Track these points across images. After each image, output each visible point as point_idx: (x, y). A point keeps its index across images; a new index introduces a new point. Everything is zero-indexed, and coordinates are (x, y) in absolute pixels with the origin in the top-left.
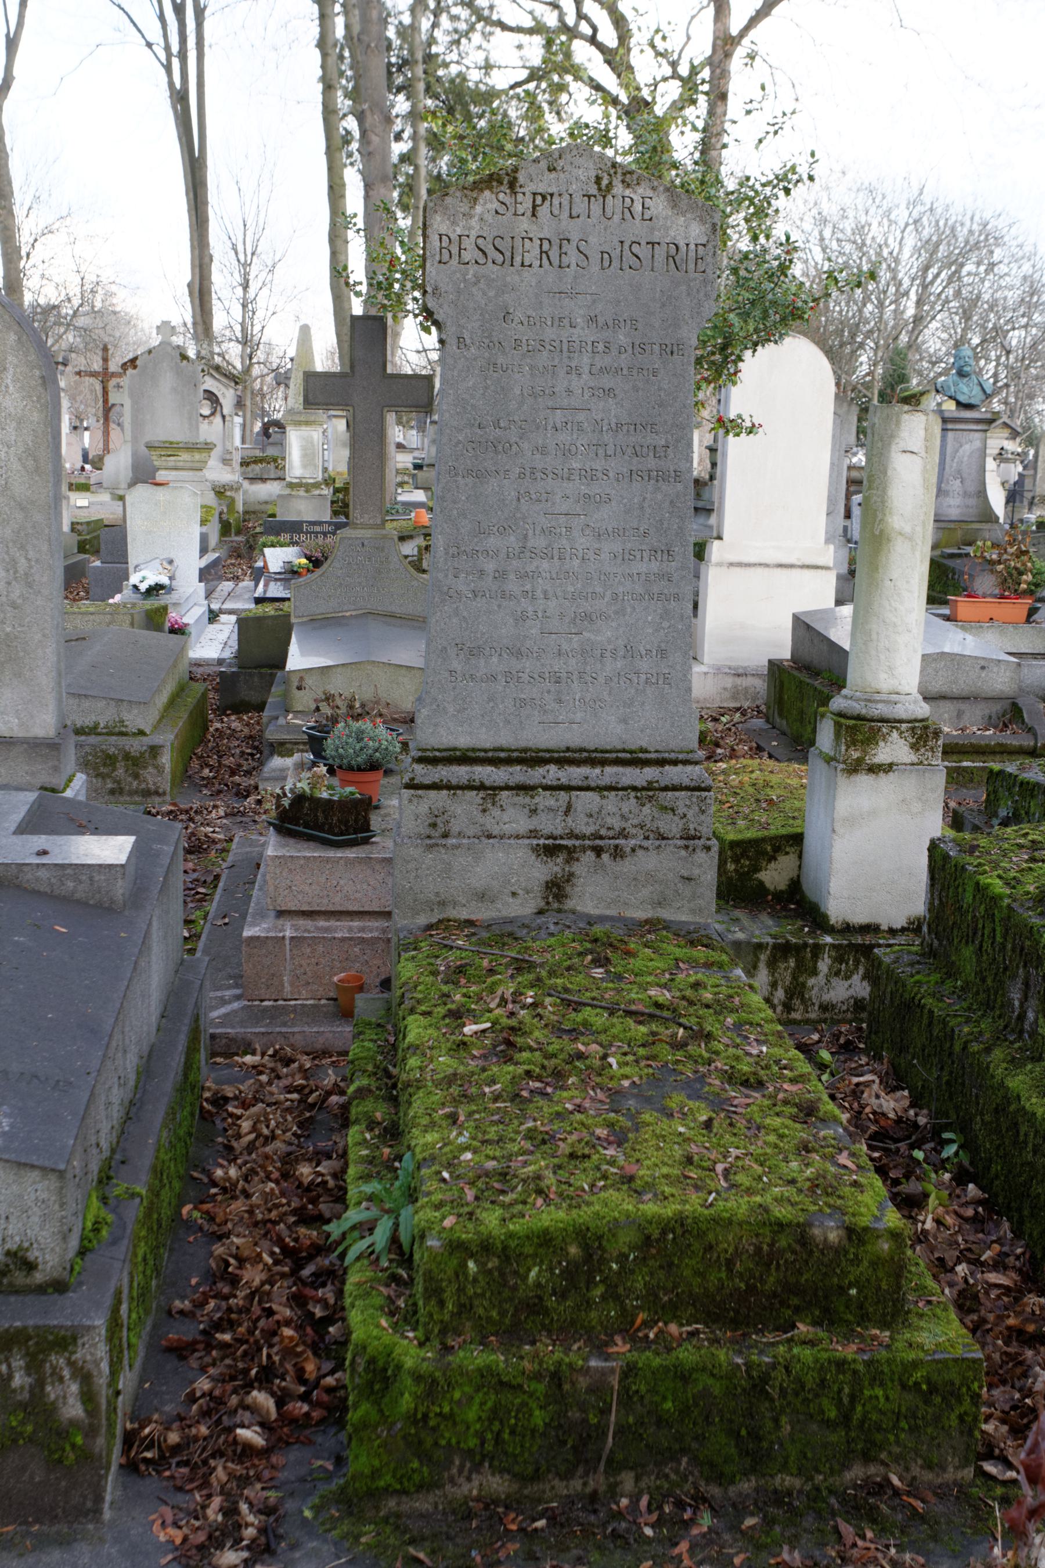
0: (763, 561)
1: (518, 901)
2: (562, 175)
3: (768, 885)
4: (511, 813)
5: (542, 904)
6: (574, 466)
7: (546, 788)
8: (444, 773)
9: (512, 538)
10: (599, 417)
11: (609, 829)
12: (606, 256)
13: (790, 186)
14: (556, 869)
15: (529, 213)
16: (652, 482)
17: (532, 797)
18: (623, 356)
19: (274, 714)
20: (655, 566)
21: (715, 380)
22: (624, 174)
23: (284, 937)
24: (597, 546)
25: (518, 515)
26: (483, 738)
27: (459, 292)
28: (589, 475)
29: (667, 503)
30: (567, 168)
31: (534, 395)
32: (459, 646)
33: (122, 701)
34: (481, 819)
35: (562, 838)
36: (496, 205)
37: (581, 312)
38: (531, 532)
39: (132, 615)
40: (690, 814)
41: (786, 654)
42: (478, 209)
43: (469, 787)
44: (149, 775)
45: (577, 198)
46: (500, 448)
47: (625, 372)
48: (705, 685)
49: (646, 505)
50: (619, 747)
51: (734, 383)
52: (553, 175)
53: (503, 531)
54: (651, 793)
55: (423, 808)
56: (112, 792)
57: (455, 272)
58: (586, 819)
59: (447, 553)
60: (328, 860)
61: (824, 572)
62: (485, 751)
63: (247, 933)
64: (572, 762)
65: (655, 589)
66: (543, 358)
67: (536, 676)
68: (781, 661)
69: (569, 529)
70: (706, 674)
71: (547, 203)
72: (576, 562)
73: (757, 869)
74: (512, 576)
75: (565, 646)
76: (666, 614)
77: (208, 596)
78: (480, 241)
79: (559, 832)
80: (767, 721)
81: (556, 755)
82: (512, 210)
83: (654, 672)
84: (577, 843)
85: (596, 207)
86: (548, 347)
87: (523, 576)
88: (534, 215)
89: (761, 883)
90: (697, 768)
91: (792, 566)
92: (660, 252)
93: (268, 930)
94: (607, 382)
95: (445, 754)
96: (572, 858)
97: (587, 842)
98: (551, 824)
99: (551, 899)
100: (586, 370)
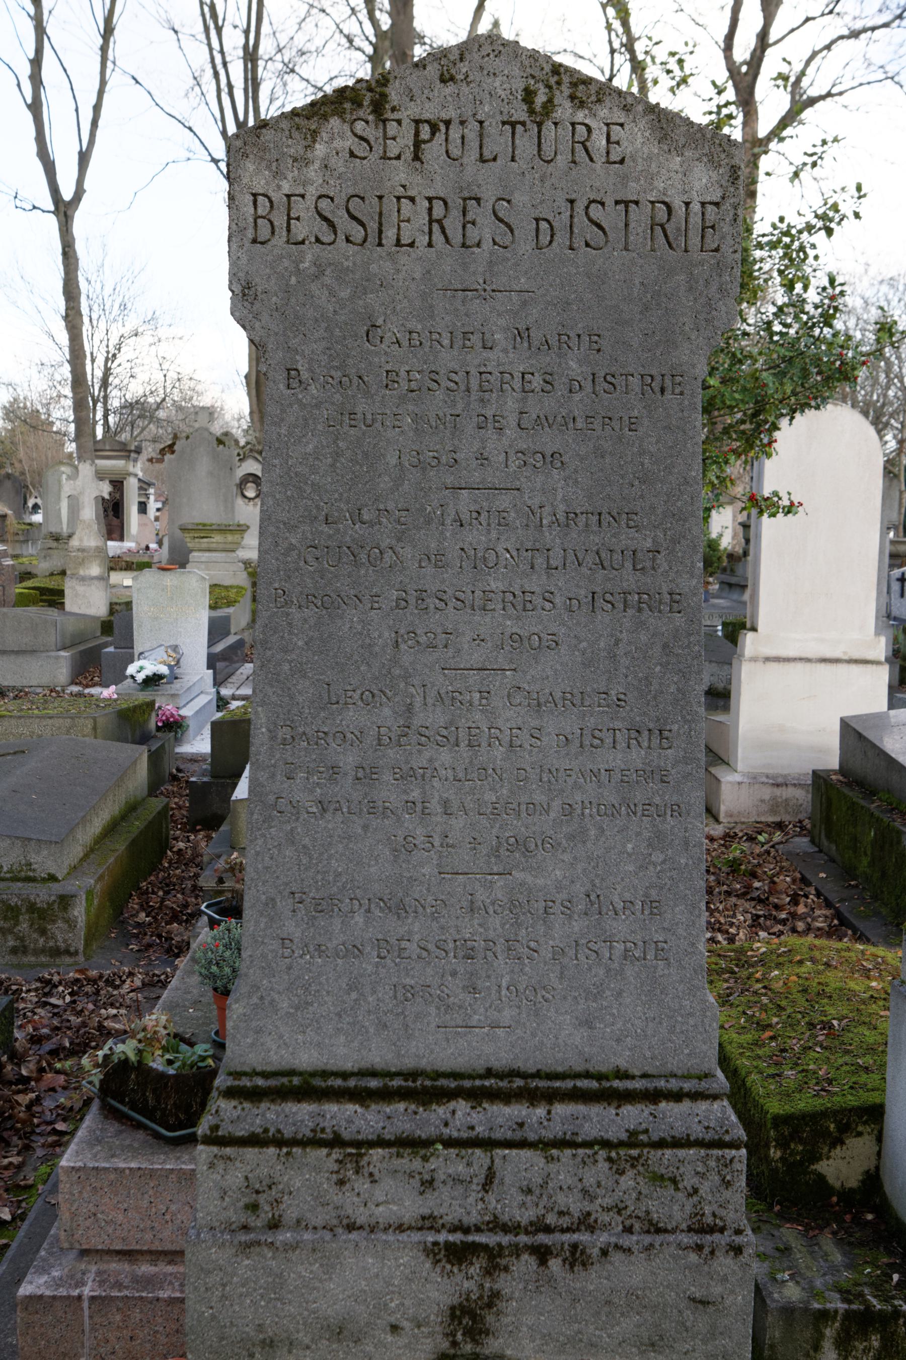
0: (803, 655)
1: (402, 1341)
2: (465, 89)
3: (831, 1180)
4: (387, 1184)
5: (445, 1345)
6: (493, 586)
7: (450, 1143)
8: (271, 1116)
9: (387, 711)
10: (535, 502)
11: (561, 1213)
12: (544, 225)
13: (833, 225)
14: (466, 1284)
15: (408, 155)
16: (631, 612)
17: (425, 1159)
18: (577, 397)
19: (217, 851)
20: (637, 757)
21: (745, 452)
22: (574, 85)
23: (80, 1297)
24: (535, 723)
25: (397, 672)
26: (343, 1054)
27: (287, 291)
28: (521, 602)
29: (657, 649)
30: (474, 76)
31: (421, 466)
32: (297, 897)
33: (30, 839)
34: (335, 1196)
35: (478, 1229)
36: (350, 142)
37: (502, 322)
38: (418, 700)
39: (95, 719)
40: (705, 1189)
41: (833, 763)
42: (320, 149)
43: (314, 1142)
44: (59, 932)
45: (492, 127)
46: (363, 557)
47: (580, 424)
48: (737, 795)
49: (620, 651)
50: (579, 1067)
51: (769, 456)
52: (450, 88)
53: (370, 699)
54: (634, 1152)
55: (235, 1177)
56: (14, 951)
57: (281, 257)
58: (521, 1198)
59: (273, 738)
60: (152, 1173)
61: (874, 666)
62: (345, 1075)
63: (25, 1290)
64: (494, 1096)
65: (639, 796)
66: (437, 403)
67: (431, 947)
68: (828, 771)
69: (485, 694)
70: (739, 783)
71: (440, 137)
72: (499, 752)
73: (815, 1158)
74: (387, 777)
75: (481, 896)
76: (658, 840)
77: (218, 683)
78: (324, 204)
79: (473, 1218)
80: (812, 841)
81: (467, 1084)
82: (378, 150)
83: (638, 938)
84: (505, 1240)
85: (526, 143)
86: (445, 383)
87: (406, 775)
88: (417, 158)
89: (821, 1178)
90: (716, 1105)
91: (837, 661)
92: (640, 218)
93: (58, 1283)
94: (549, 441)
95: (272, 1082)
96: (496, 1267)
97: (523, 1239)
98: (458, 1206)
99: (459, 1337)
100: (512, 420)
